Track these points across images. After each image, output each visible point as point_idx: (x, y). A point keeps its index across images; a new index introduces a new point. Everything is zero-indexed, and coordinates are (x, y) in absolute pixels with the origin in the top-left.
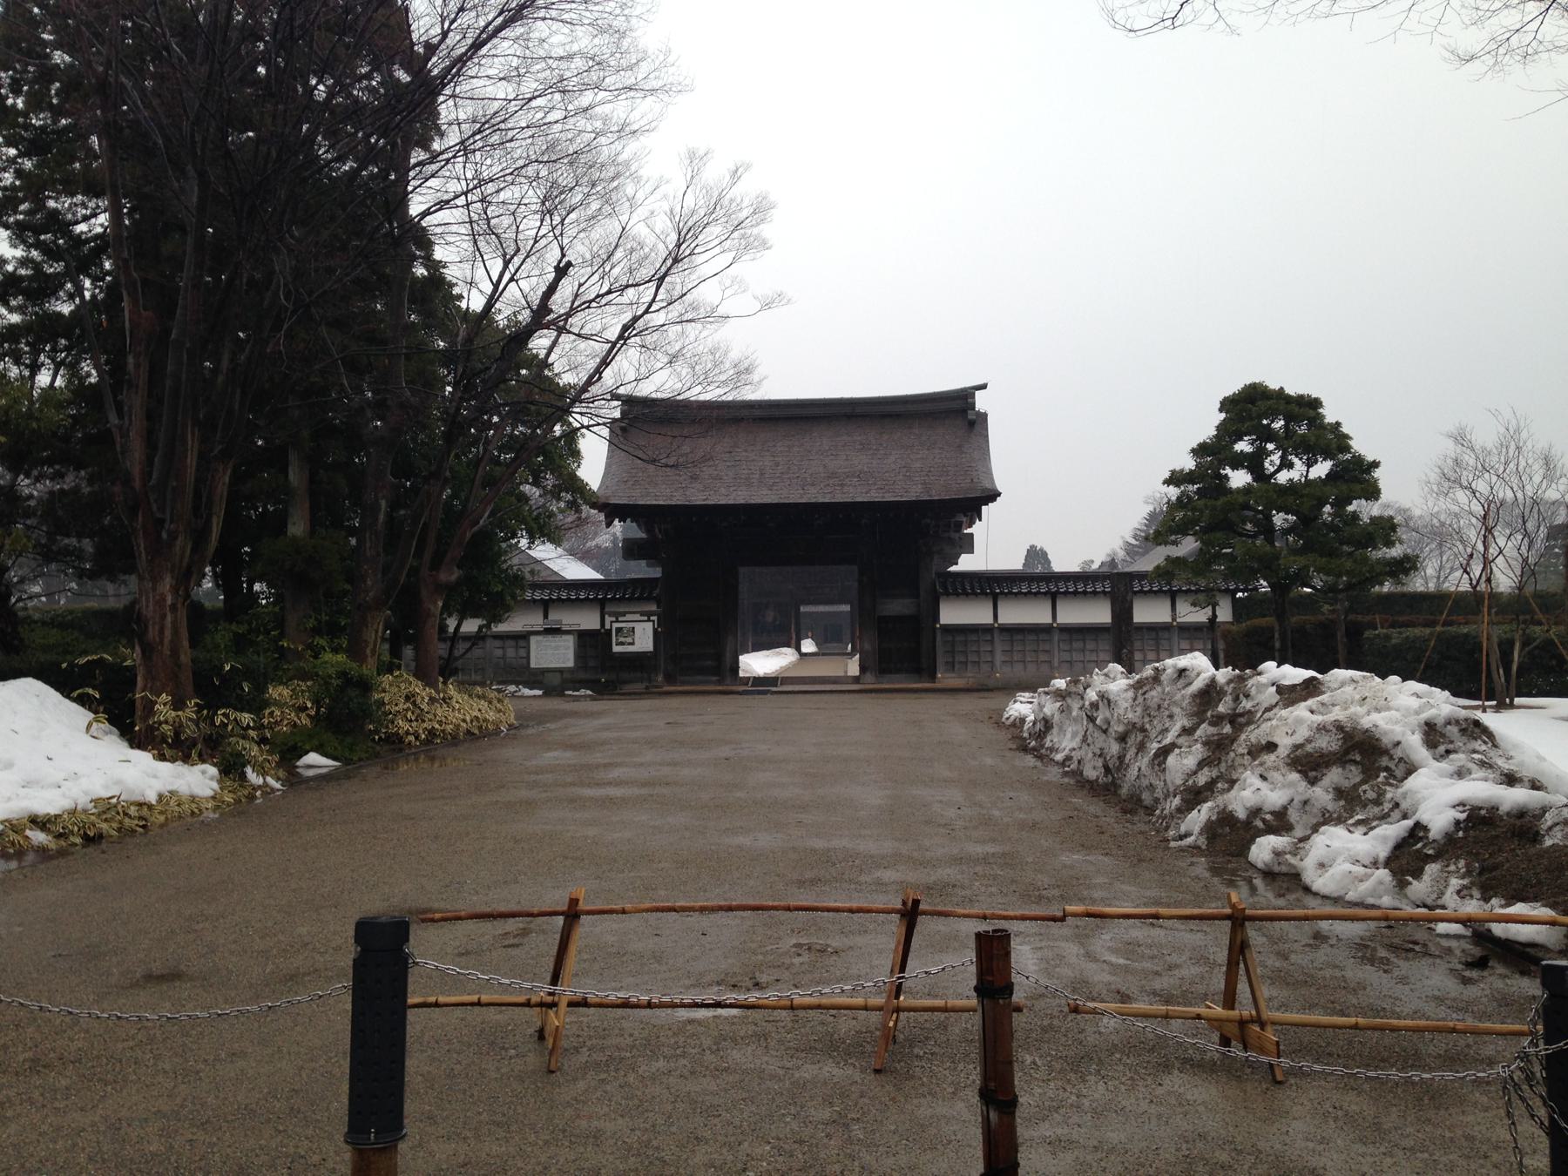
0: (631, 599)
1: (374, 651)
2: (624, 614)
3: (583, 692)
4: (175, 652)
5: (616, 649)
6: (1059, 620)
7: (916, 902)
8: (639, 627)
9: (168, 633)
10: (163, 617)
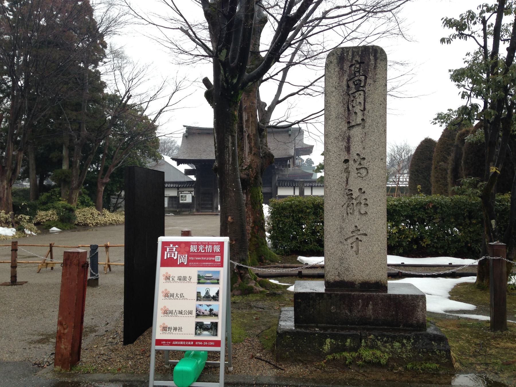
0: (188, 187)
1: (75, 201)
2: (183, 191)
3: (171, 214)
4: (7, 200)
5: (181, 202)
6: (313, 194)
7: (17, 242)
8: (187, 195)
9: (5, 195)
10: (4, 191)
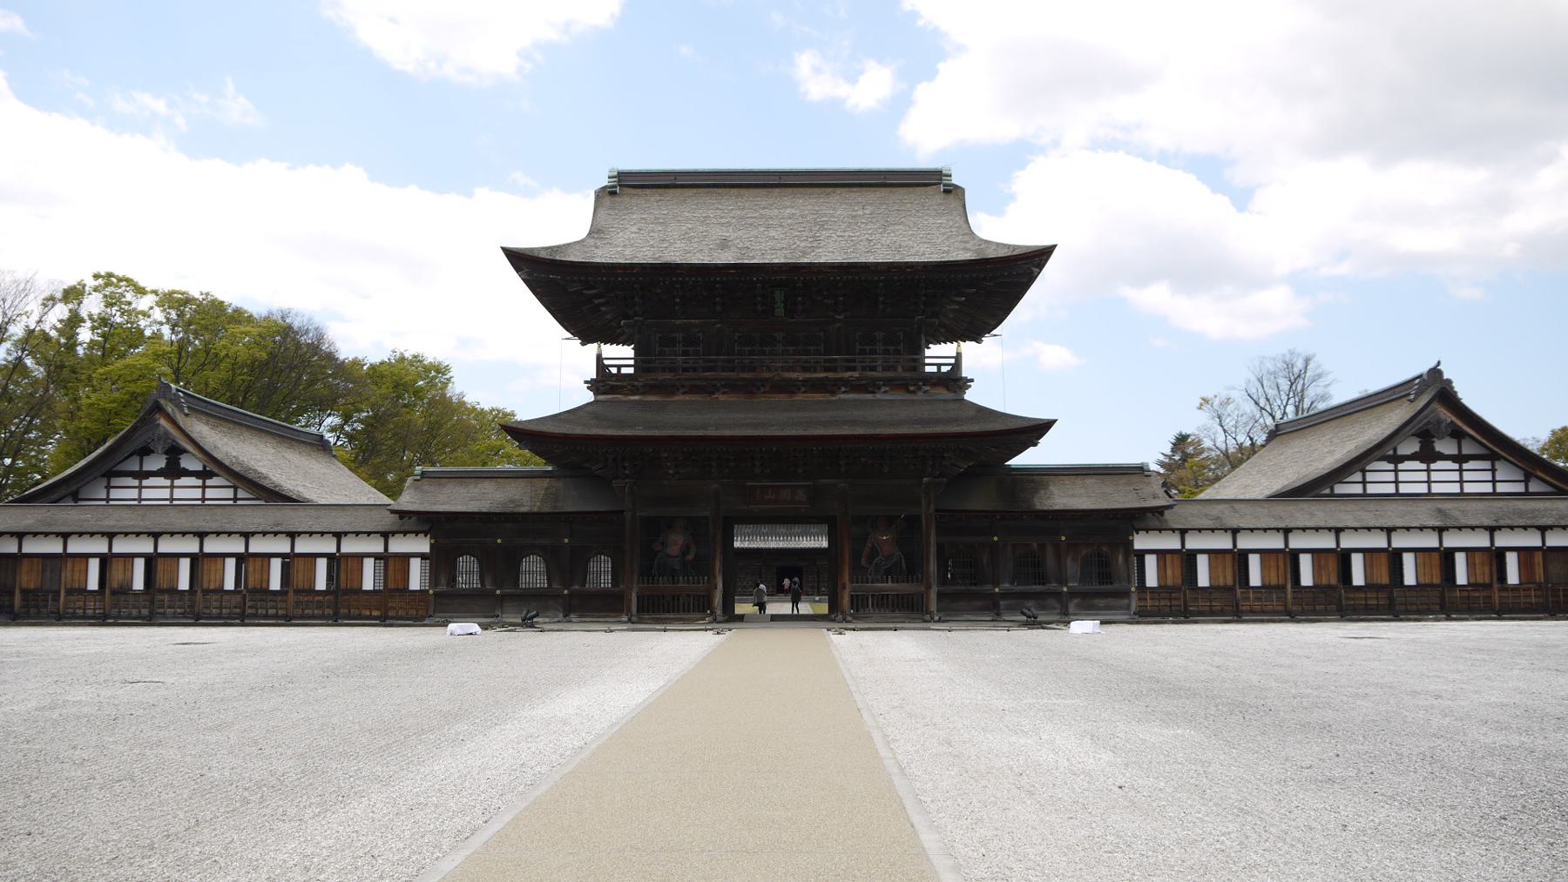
5: (737, 544)
